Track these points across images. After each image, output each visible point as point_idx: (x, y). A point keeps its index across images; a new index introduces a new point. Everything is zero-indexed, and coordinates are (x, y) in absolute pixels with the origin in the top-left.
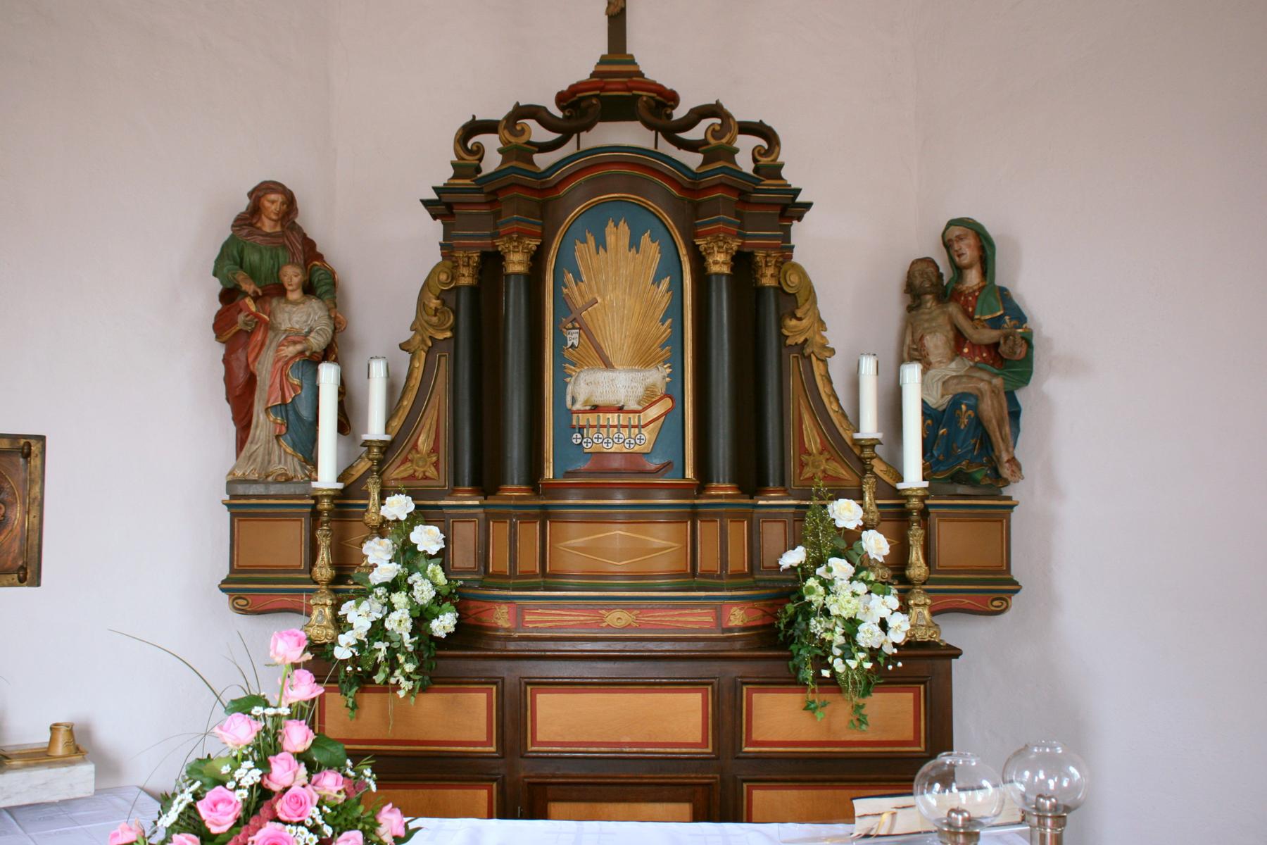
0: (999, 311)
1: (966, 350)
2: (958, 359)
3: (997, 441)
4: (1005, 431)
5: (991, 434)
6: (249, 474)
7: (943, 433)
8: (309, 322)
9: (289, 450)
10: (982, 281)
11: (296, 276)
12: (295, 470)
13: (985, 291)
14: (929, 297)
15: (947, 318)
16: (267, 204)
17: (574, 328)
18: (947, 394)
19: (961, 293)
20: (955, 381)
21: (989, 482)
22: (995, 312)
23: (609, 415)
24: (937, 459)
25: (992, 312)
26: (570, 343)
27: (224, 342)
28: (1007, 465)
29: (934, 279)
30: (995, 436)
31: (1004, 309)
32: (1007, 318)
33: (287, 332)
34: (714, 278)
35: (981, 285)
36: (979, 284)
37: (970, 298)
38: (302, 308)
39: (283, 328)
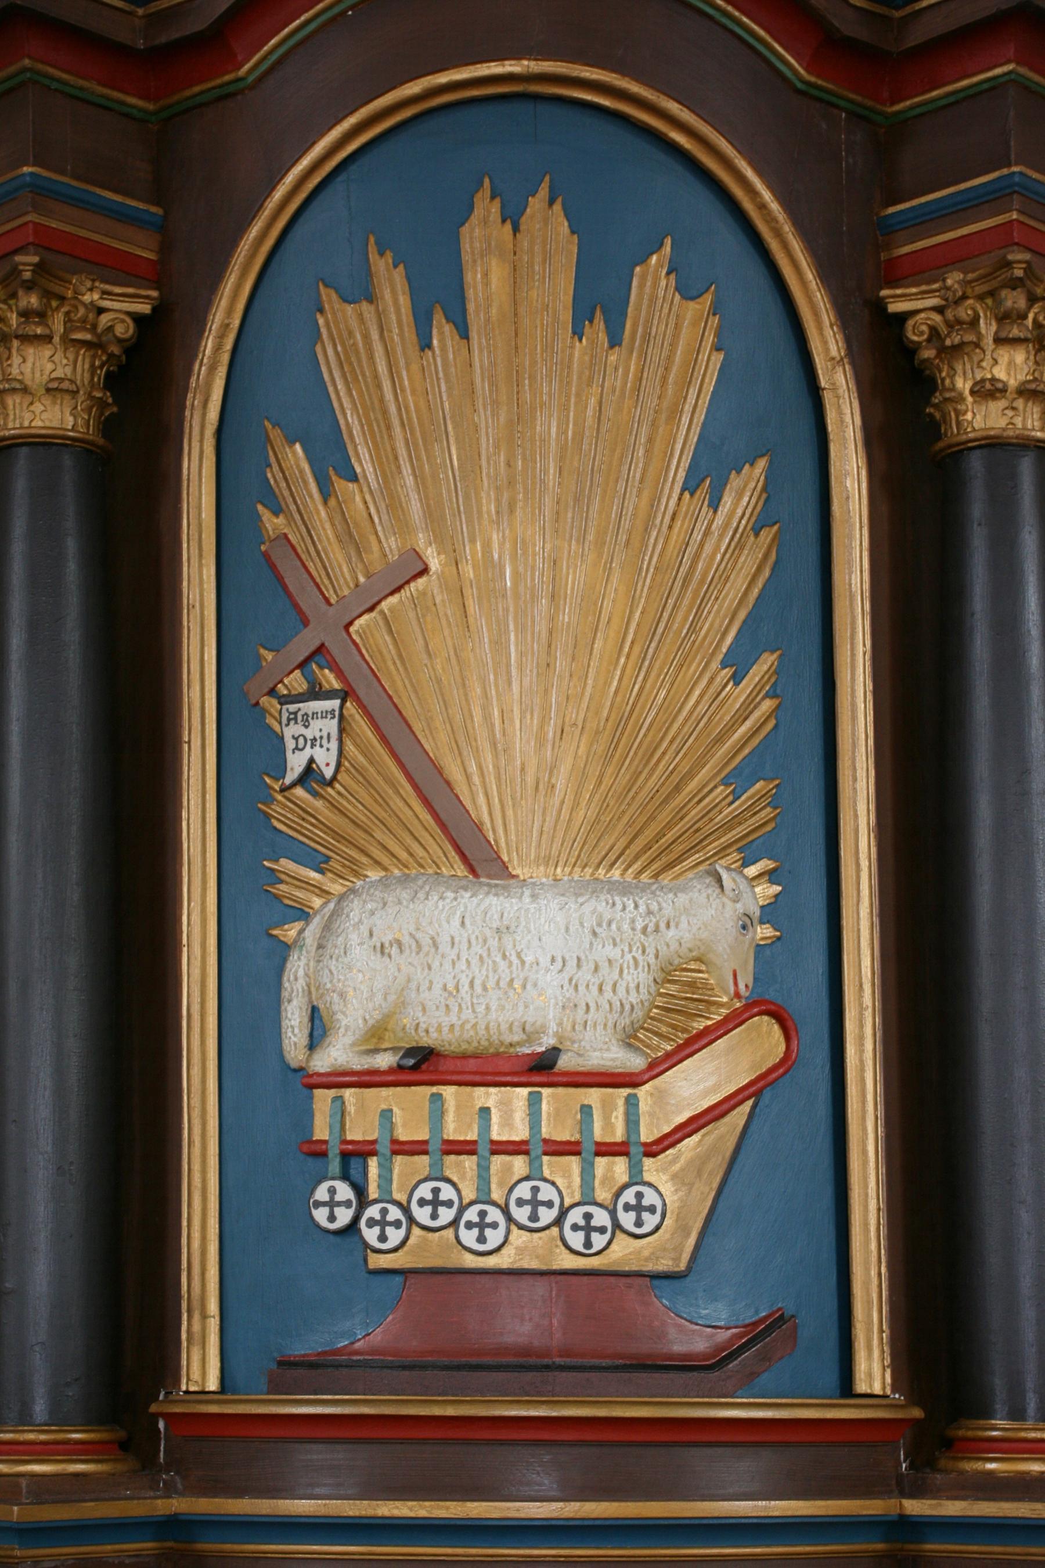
17: (316, 692)
23: (489, 1097)
26: (296, 763)
34: (976, 464)
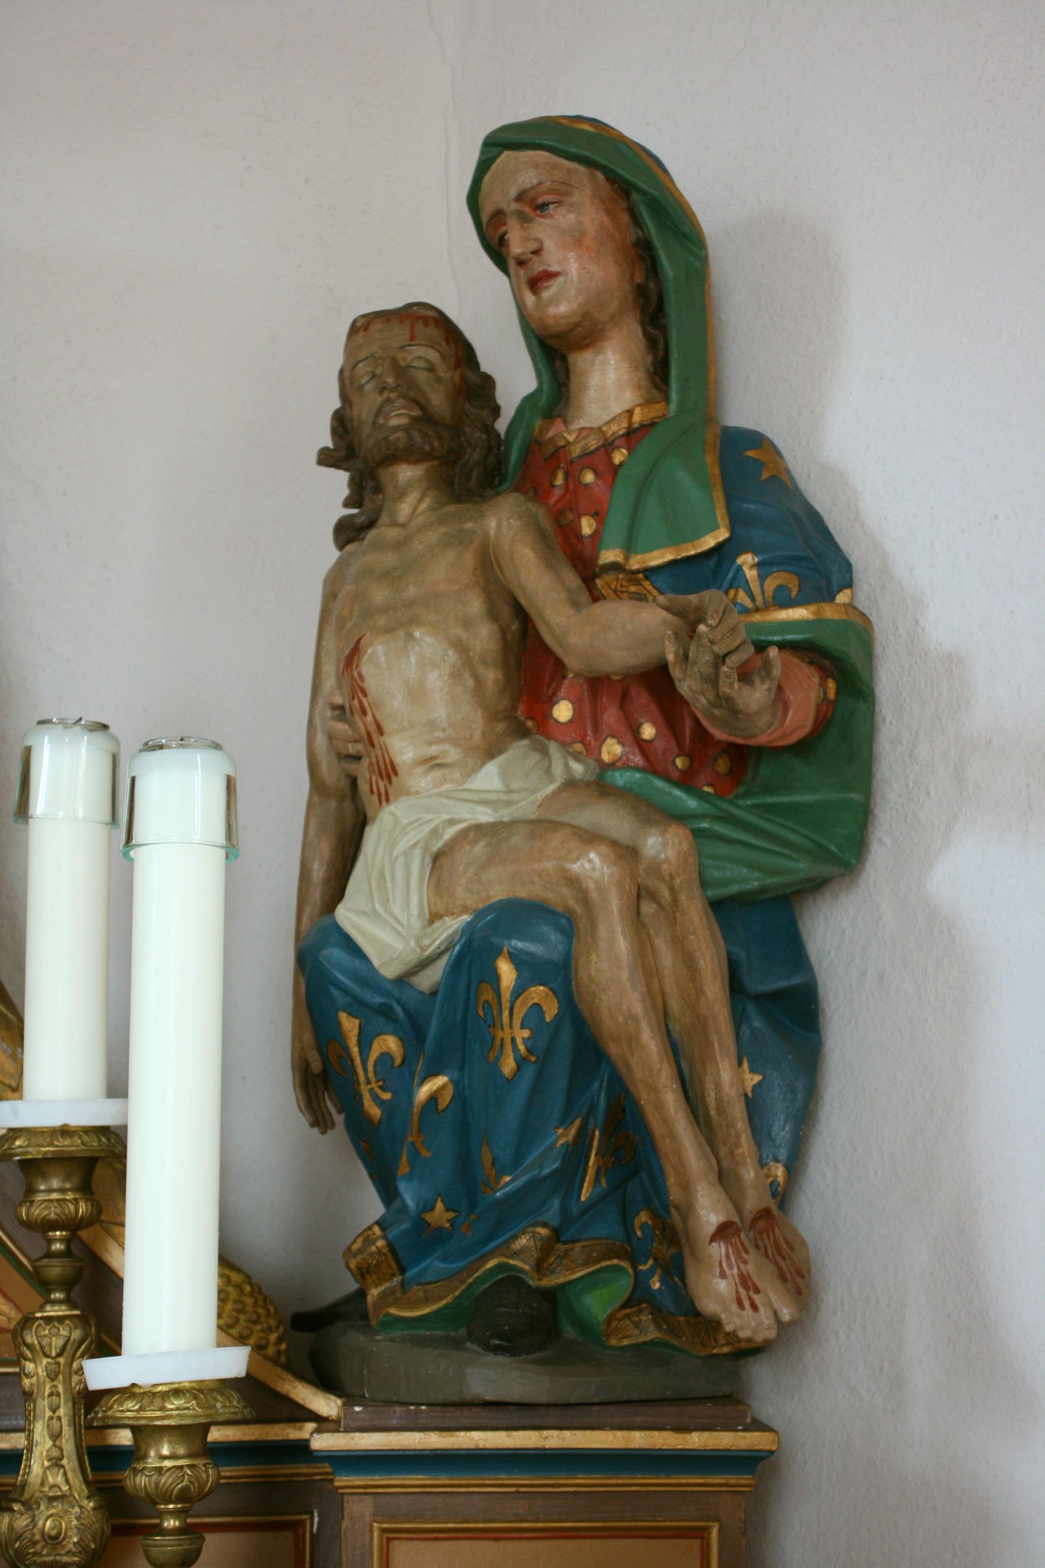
0: (714, 527)
1: (563, 711)
2: (519, 748)
3: (673, 1136)
4: (718, 1085)
5: (644, 1098)
7: (433, 1098)
10: (647, 403)
13: (647, 447)
14: (406, 473)
15: (469, 559)
18: (450, 913)
19: (556, 456)
20: (479, 849)
21: (652, 1334)
22: (698, 534)
24: (421, 1225)
25: (677, 538)
28: (718, 1250)
29: (438, 400)
30: (659, 1106)
31: (735, 521)
32: (747, 560)
35: (637, 418)
36: (630, 412)
37: (589, 477)
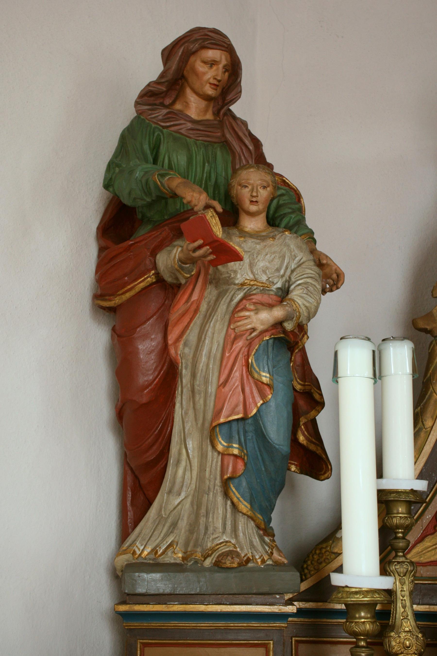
6: (163, 553)
8: (282, 272)
9: (244, 506)
11: (265, 187)
12: (252, 546)
16: (201, 67)
27: (112, 310)
33: (246, 288)
38: (270, 246)
39: (239, 279)
